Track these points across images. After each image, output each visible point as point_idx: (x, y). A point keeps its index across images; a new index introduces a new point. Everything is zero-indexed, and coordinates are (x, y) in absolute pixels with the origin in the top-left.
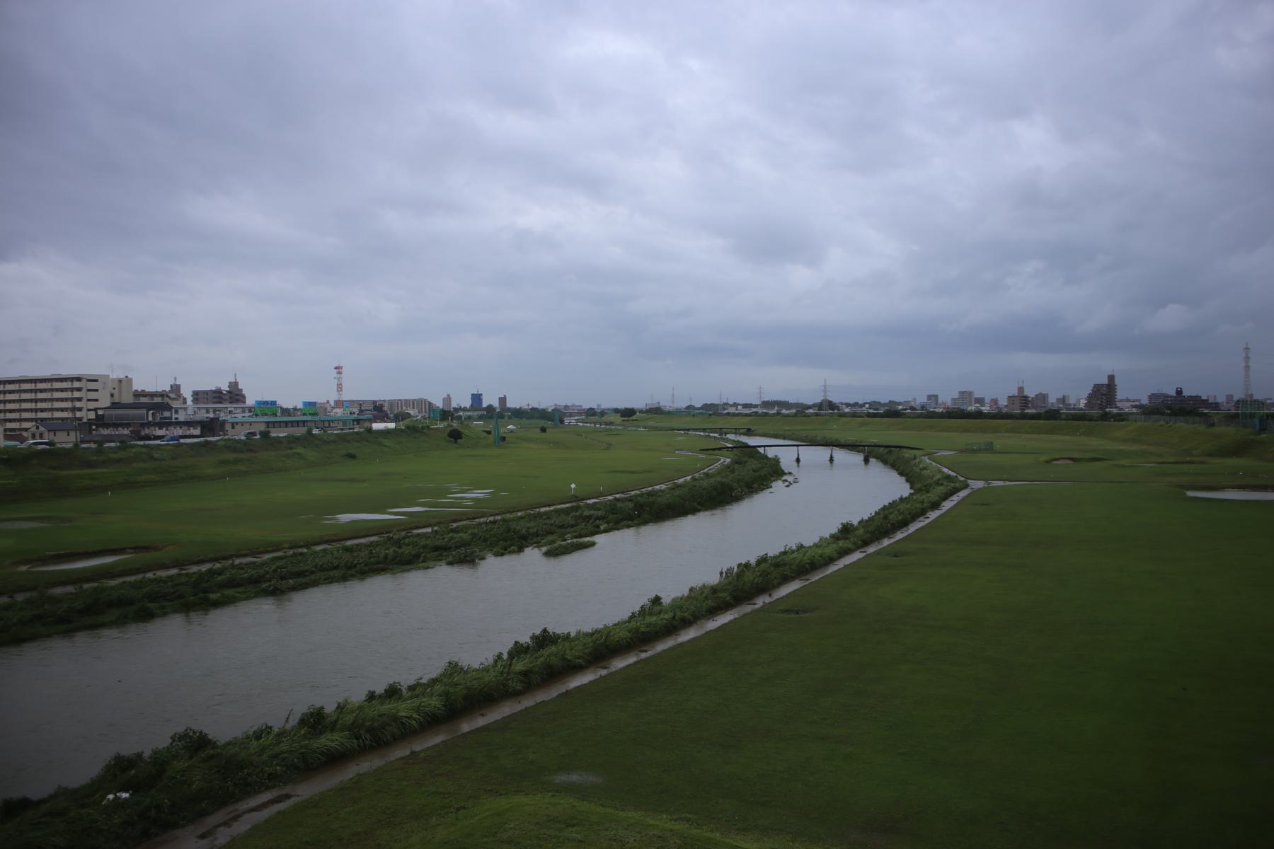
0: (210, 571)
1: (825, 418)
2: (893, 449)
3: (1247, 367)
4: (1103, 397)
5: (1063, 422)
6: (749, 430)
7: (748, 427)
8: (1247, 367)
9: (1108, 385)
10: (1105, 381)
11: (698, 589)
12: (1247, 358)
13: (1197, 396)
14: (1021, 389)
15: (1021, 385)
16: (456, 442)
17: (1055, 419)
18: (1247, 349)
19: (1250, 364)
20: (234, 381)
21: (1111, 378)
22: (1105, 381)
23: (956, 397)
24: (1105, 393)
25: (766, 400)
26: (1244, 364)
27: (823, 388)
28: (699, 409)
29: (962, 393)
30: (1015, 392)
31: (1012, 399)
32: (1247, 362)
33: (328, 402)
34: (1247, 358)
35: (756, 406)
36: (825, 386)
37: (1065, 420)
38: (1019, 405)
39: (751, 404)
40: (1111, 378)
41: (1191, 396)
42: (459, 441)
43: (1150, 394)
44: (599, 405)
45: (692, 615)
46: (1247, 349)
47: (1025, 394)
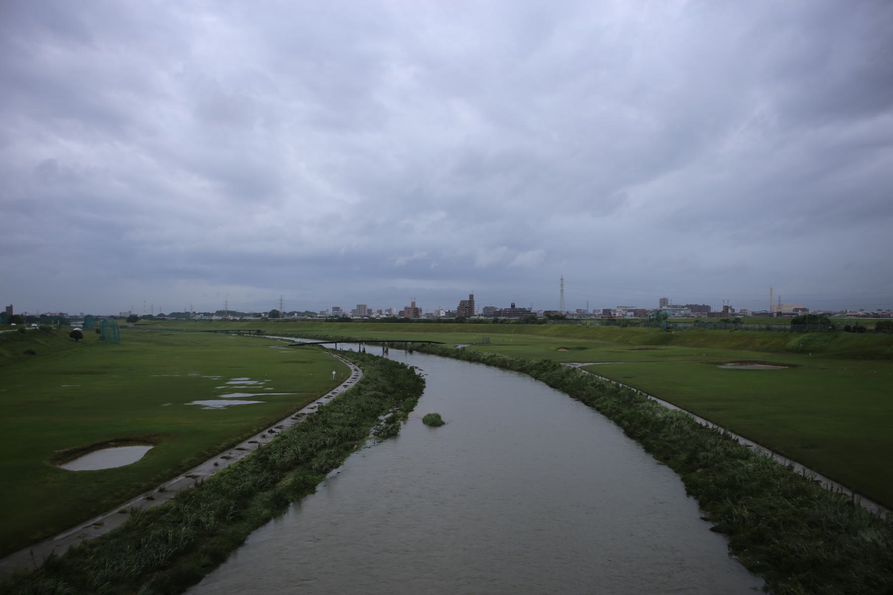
0: (504, 319)
1: (310, 322)
2: (424, 343)
3: (562, 291)
4: (467, 309)
5: (468, 324)
6: (259, 331)
7: (258, 329)
8: (562, 291)
9: (470, 301)
10: (468, 299)
11: (408, 368)
12: (562, 285)
13: (524, 309)
14: (413, 304)
15: (413, 301)
16: (77, 340)
17: (462, 322)
18: (562, 279)
19: (564, 289)
20: (586, 309)
21: (471, 296)
22: (468, 299)
23: (355, 309)
24: (468, 306)
25: (229, 310)
26: (560, 289)
27: (280, 302)
28: (168, 316)
29: (359, 306)
30: (410, 305)
31: (408, 310)
32: (562, 282)
33: (328, 310)
34: (562, 285)
35: (213, 315)
36: (281, 300)
37: (468, 323)
38: (412, 312)
39: (209, 313)
40: (471, 296)
41: (521, 309)
42: (80, 340)
43: (484, 307)
44: (81, 313)
45: (546, 315)
46: (562, 279)
47: (416, 306)
